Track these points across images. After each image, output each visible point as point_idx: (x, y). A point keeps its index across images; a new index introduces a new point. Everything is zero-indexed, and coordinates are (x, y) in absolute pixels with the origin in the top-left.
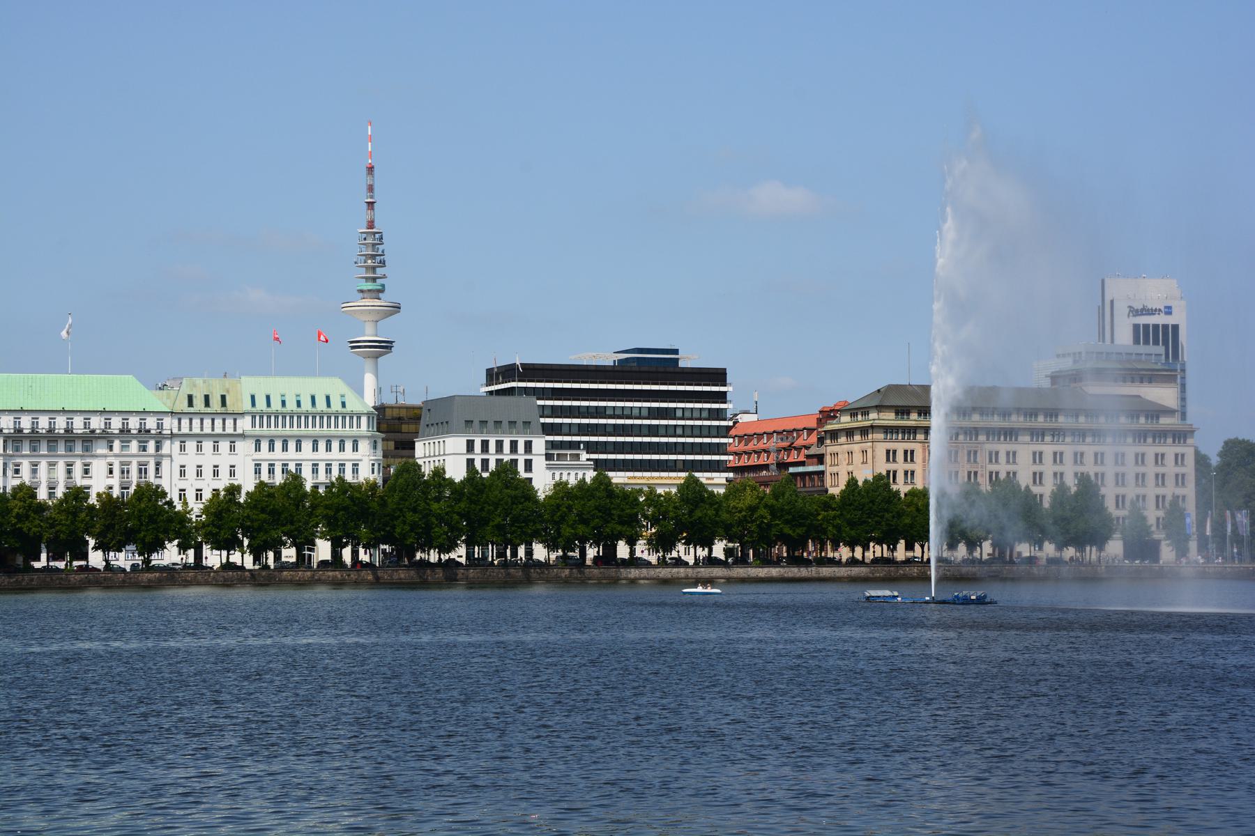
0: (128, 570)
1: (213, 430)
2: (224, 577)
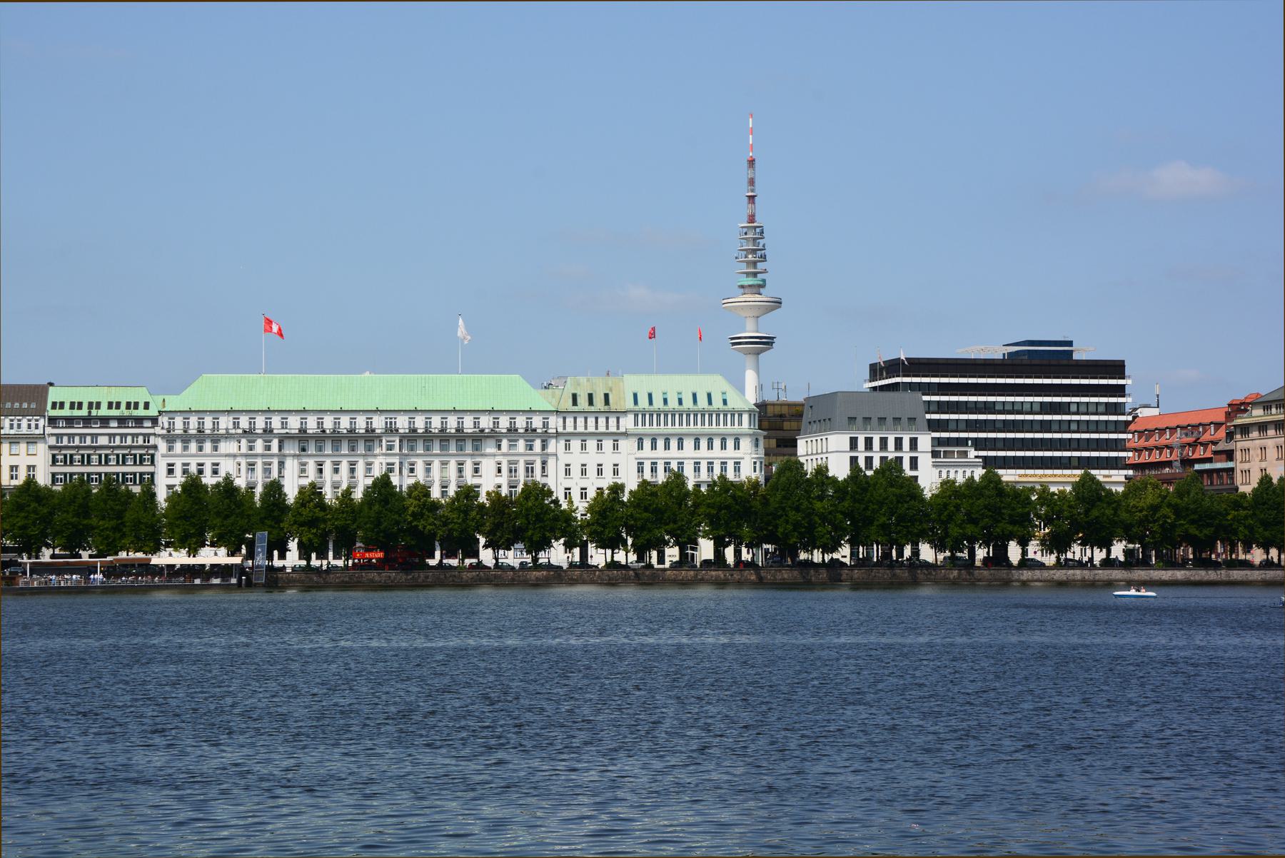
2: (608, 576)
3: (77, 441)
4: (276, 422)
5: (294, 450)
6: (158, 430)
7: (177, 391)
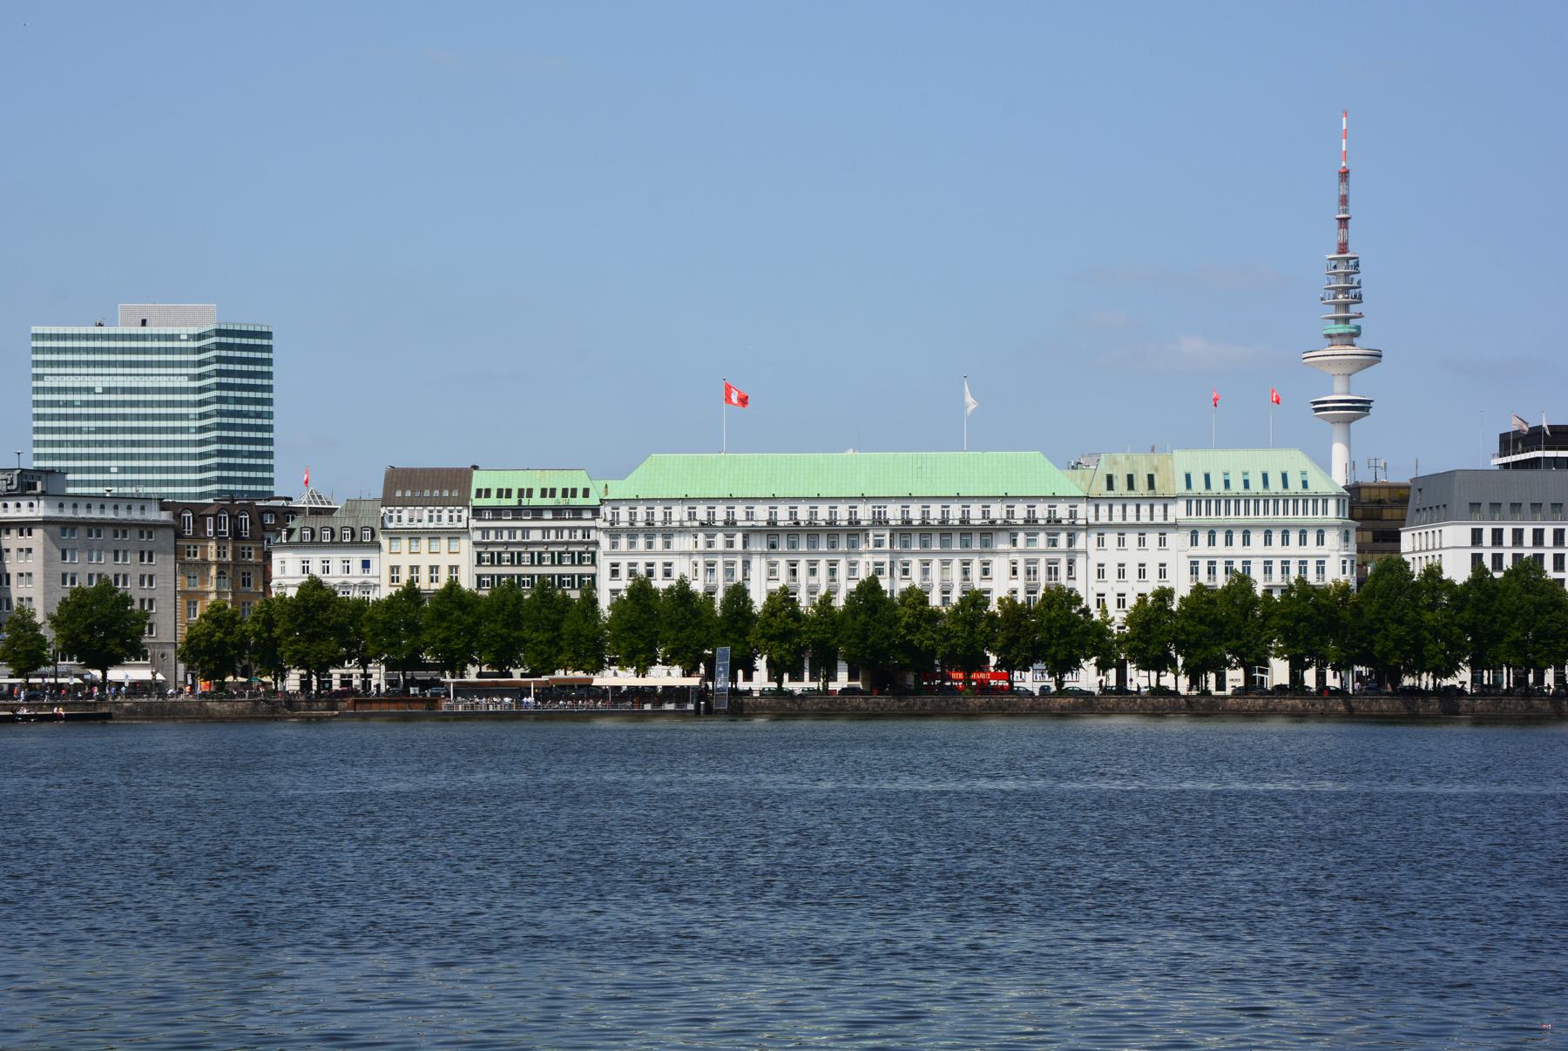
0: (1037, 694)
2: (1153, 704)
4: (740, 513)
6: (599, 523)
7: (622, 475)
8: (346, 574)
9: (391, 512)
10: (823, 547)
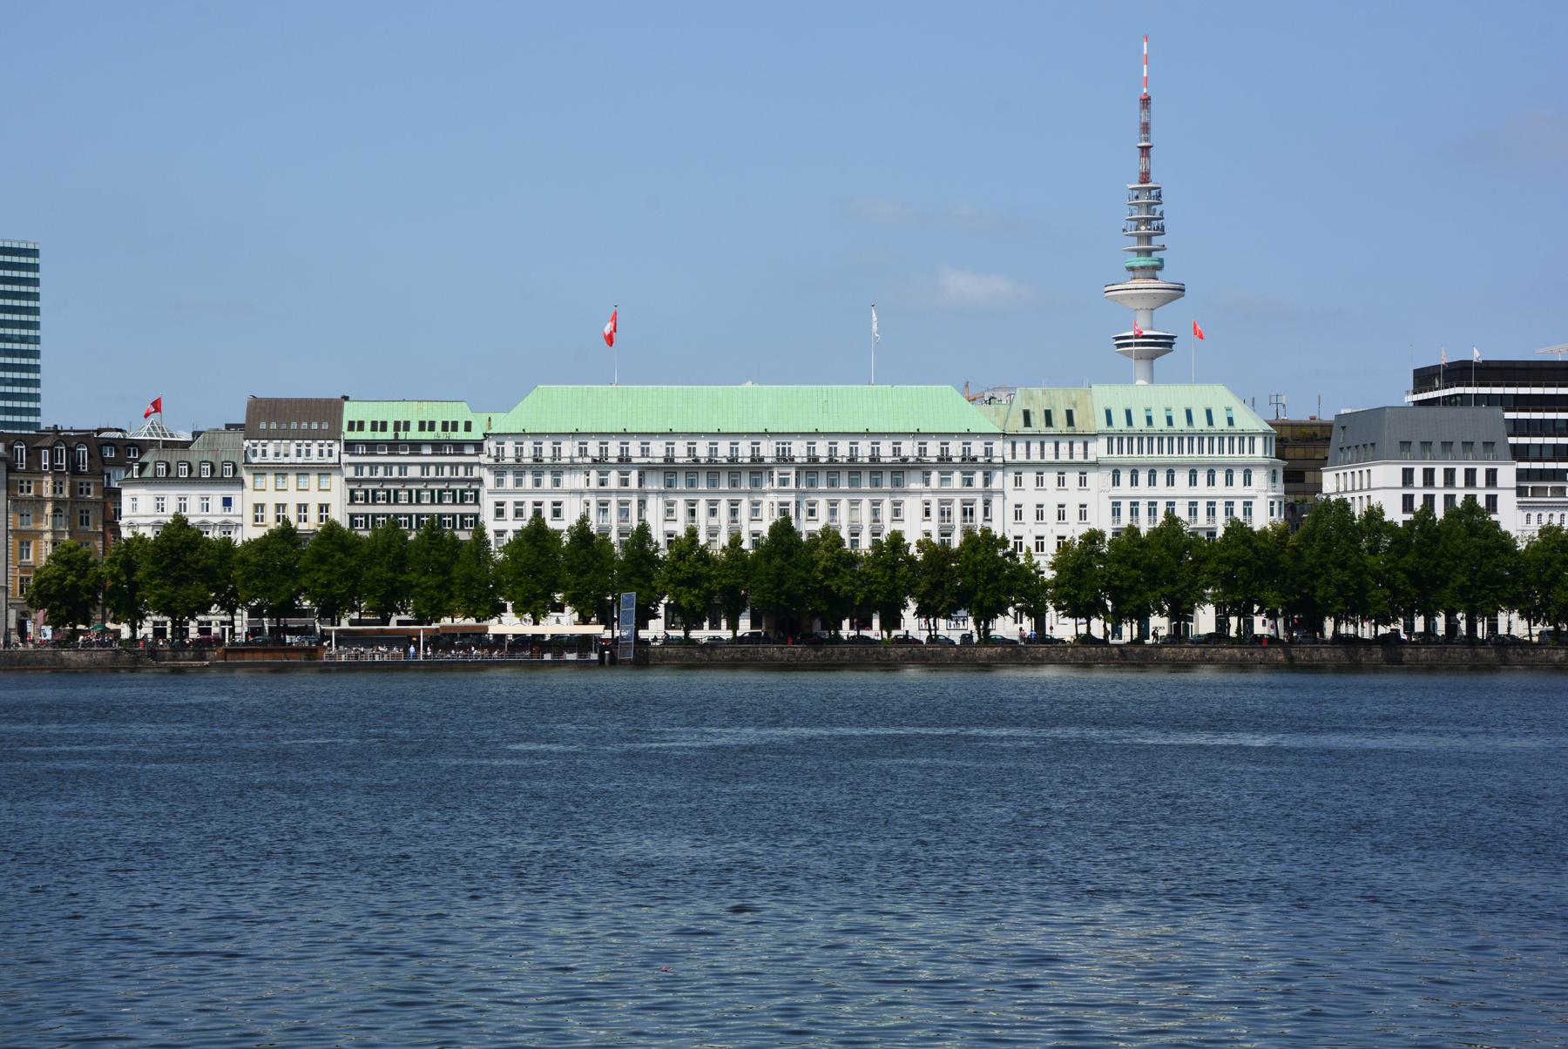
0: (958, 643)
1: (1057, 457)
2: (1085, 653)
3: (380, 474)
4: (634, 449)
5: (658, 485)
6: (483, 459)
7: (507, 408)
8: (205, 513)
9: (255, 445)
10: (724, 486)
